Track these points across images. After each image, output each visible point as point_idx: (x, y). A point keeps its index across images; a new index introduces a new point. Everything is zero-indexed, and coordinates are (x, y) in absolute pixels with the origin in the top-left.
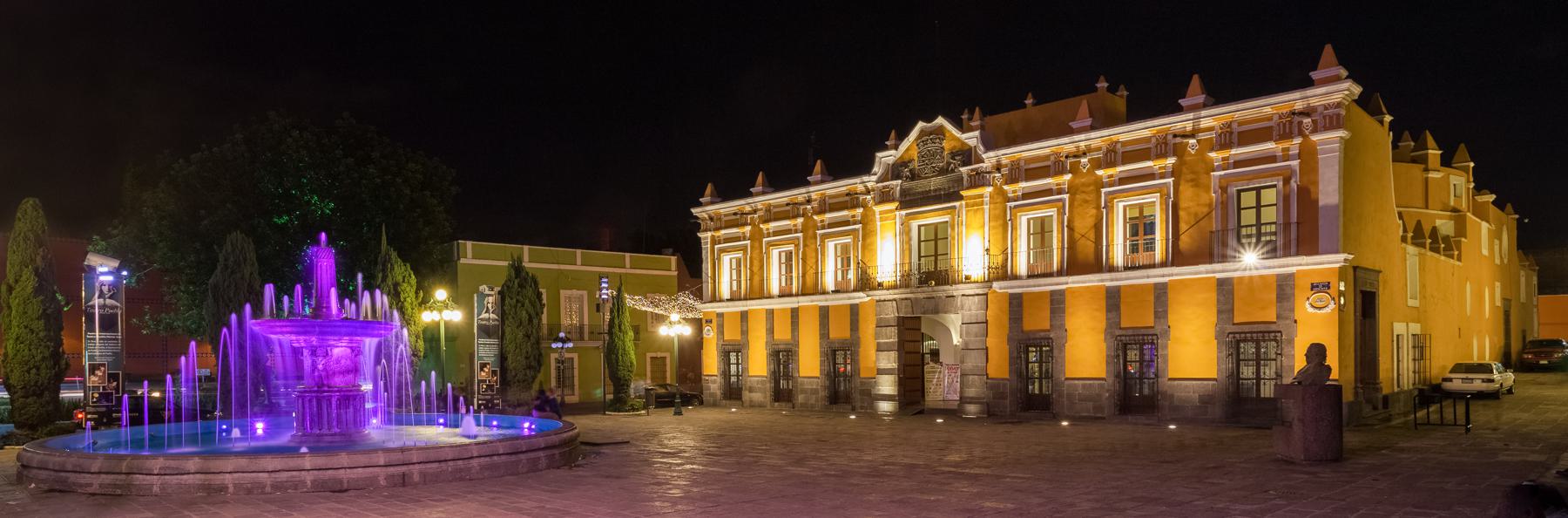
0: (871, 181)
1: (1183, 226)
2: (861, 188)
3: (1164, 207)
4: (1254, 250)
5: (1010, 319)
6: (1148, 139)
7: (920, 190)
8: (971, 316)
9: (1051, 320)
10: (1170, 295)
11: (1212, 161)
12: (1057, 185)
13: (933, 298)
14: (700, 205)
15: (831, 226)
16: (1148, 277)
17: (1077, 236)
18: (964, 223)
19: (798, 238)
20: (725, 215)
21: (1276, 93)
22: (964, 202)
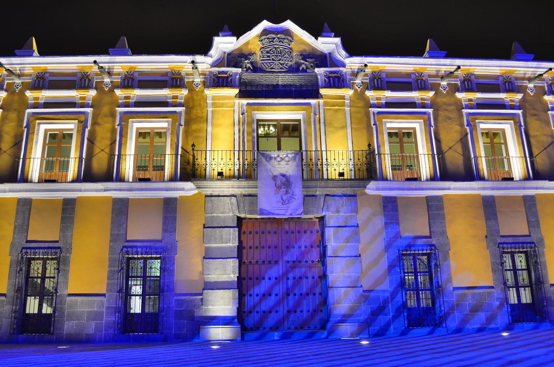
1: (535, 151)
3: (519, 132)
10: (539, 207)
11: (117, 98)
12: (422, 99)
15: (138, 104)
17: (444, 147)
18: (322, 121)
21: (53, 89)
22: (321, 101)
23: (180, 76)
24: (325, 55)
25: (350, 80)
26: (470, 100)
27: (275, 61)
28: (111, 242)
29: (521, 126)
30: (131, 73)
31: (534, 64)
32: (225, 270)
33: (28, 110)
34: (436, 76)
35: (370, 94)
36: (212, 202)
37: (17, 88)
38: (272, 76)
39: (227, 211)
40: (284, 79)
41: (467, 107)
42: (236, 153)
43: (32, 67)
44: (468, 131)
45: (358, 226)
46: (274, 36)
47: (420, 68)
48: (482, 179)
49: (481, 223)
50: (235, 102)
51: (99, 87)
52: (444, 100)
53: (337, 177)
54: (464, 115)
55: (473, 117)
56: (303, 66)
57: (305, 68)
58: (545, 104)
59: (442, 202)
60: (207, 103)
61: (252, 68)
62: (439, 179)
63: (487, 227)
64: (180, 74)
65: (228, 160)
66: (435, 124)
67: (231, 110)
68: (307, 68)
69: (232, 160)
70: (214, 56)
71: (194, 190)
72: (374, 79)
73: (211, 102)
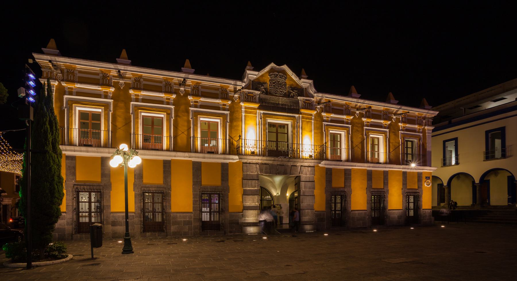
0: (240, 85)
1: (391, 150)
2: (231, 88)
4: (414, 163)
5: (326, 181)
6: (380, 111)
7: (272, 101)
8: (306, 177)
9: (345, 183)
11: (130, 95)
13: (284, 165)
14: (42, 53)
16: (385, 168)
17: (354, 146)
19: (170, 109)
20: (80, 72)
21: (110, 63)
22: (301, 116)
23: (226, 92)
24: (303, 89)
25: (316, 105)
26: (368, 122)
27: (278, 89)
28: (193, 185)
29: (387, 137)
30: (139, 79)
31: (362, 101)
32: (254, 201)
33: (132, 102)
34: (355, 108)
35: (324, 114)
36: (247, 166)
37: (122, 86)
38: (276, 98)
39: (254, 172)
40: (282, 100)
41: (367, 126)
42: (258, 141)
43: (132, 73)
44: (365, 138)
45: (314, 182)
46: (277, 73)
47: (349, 103)
48: (196, 152)
49: (365, 182)
50: (257, 111)
51: (116, 85)
52: (356, 121)
53: (308, 158)
54: (364, 129)
55: (368, 131)
56: (292, 94)
57: (293, 96)
58: (398, 127)
59: (351, 172)
60: (242, 110)
61: (265, 92)
62: (350, 161)
63: (367, 184)
64: (226, 91)
65: (254, 145)
66: (351, 133)
67: (255, 116)
68: (294, 96)
69: (256, 145)
70: (246, 82)
71: (238, 159)
72: (327, 106)
73: (244, 110)
